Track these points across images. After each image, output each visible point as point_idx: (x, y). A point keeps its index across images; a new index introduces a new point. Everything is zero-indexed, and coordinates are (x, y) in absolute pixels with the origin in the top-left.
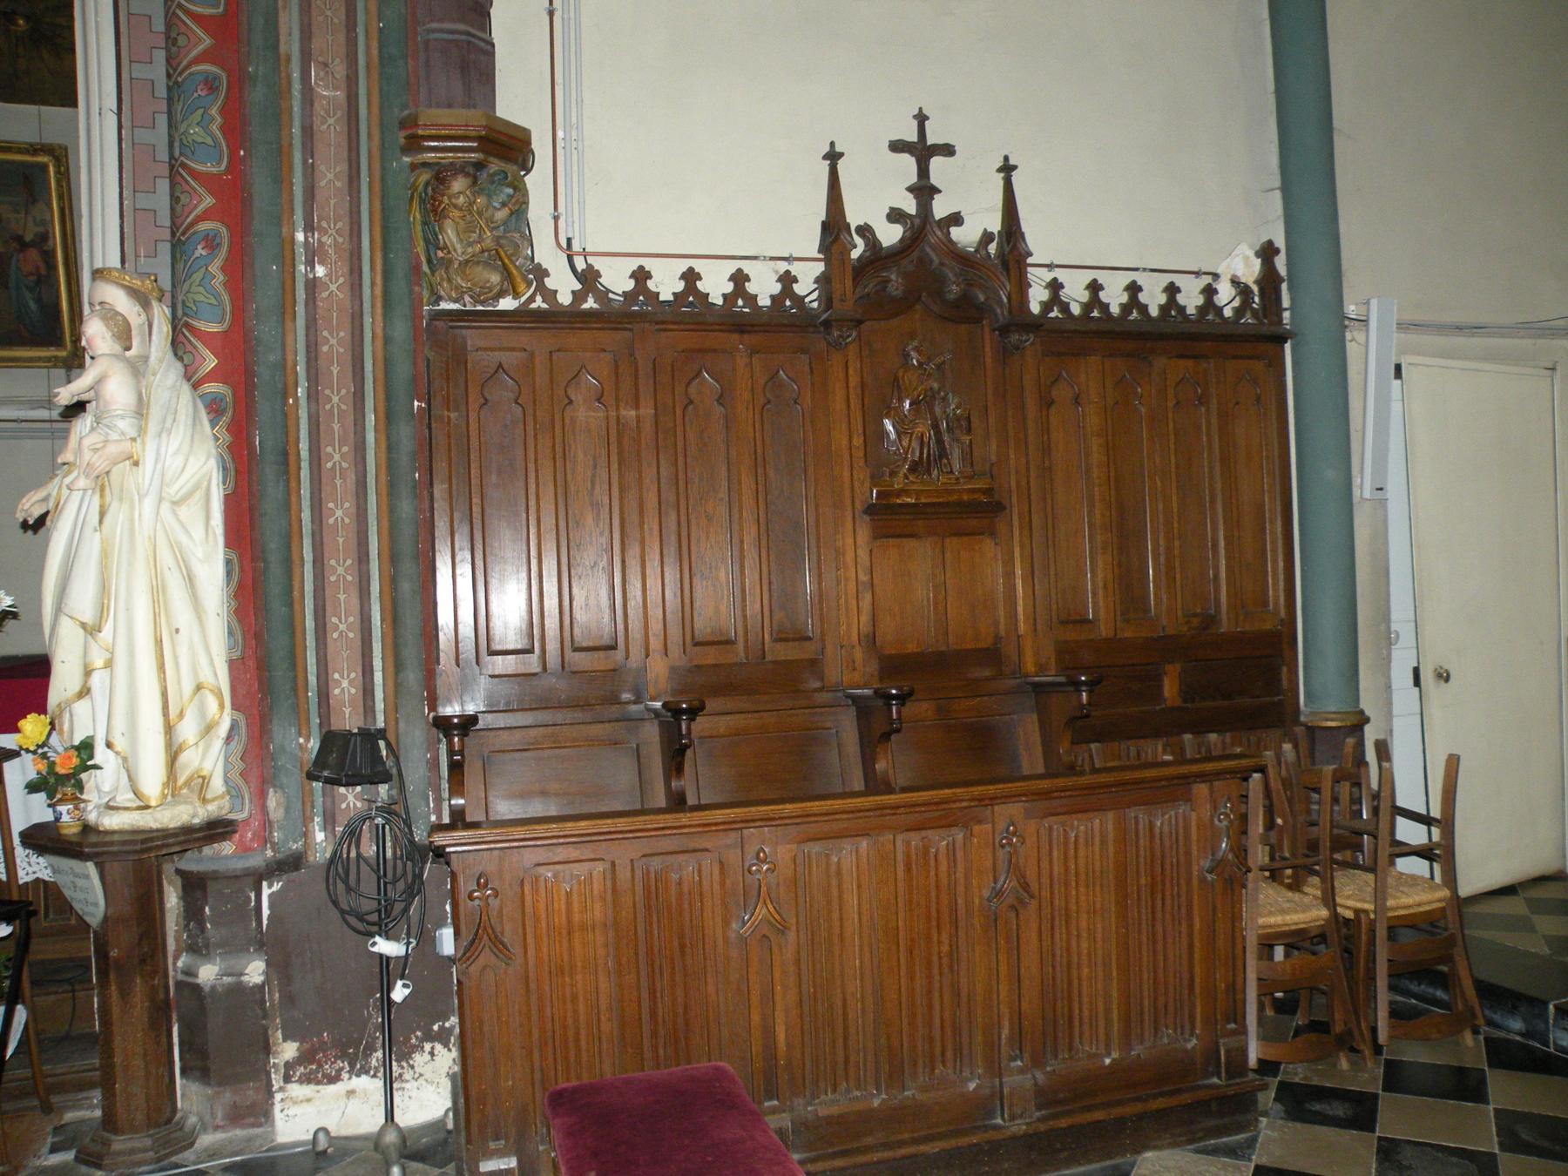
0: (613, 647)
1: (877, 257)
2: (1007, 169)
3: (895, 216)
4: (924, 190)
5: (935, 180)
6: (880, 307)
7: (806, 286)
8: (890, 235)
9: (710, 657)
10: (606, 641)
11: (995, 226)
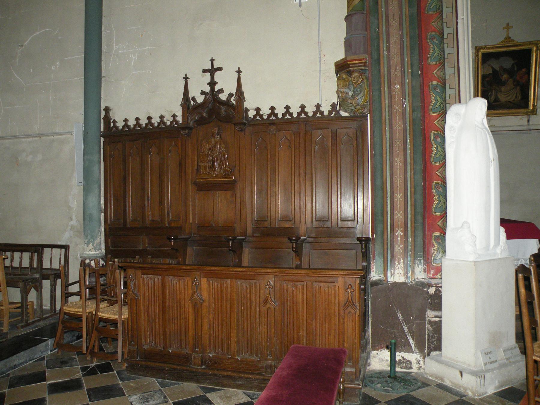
0: (327, 221)
1: (198, 107)
2: (239, 72)
3: (203, 93)
4: (212, 84)
5: (216, 80)
6: (201, 122)
7: (179, 119)
8: (200, 99)
9: (321, 224)
10: (353, 218)
11: (234, 91)
